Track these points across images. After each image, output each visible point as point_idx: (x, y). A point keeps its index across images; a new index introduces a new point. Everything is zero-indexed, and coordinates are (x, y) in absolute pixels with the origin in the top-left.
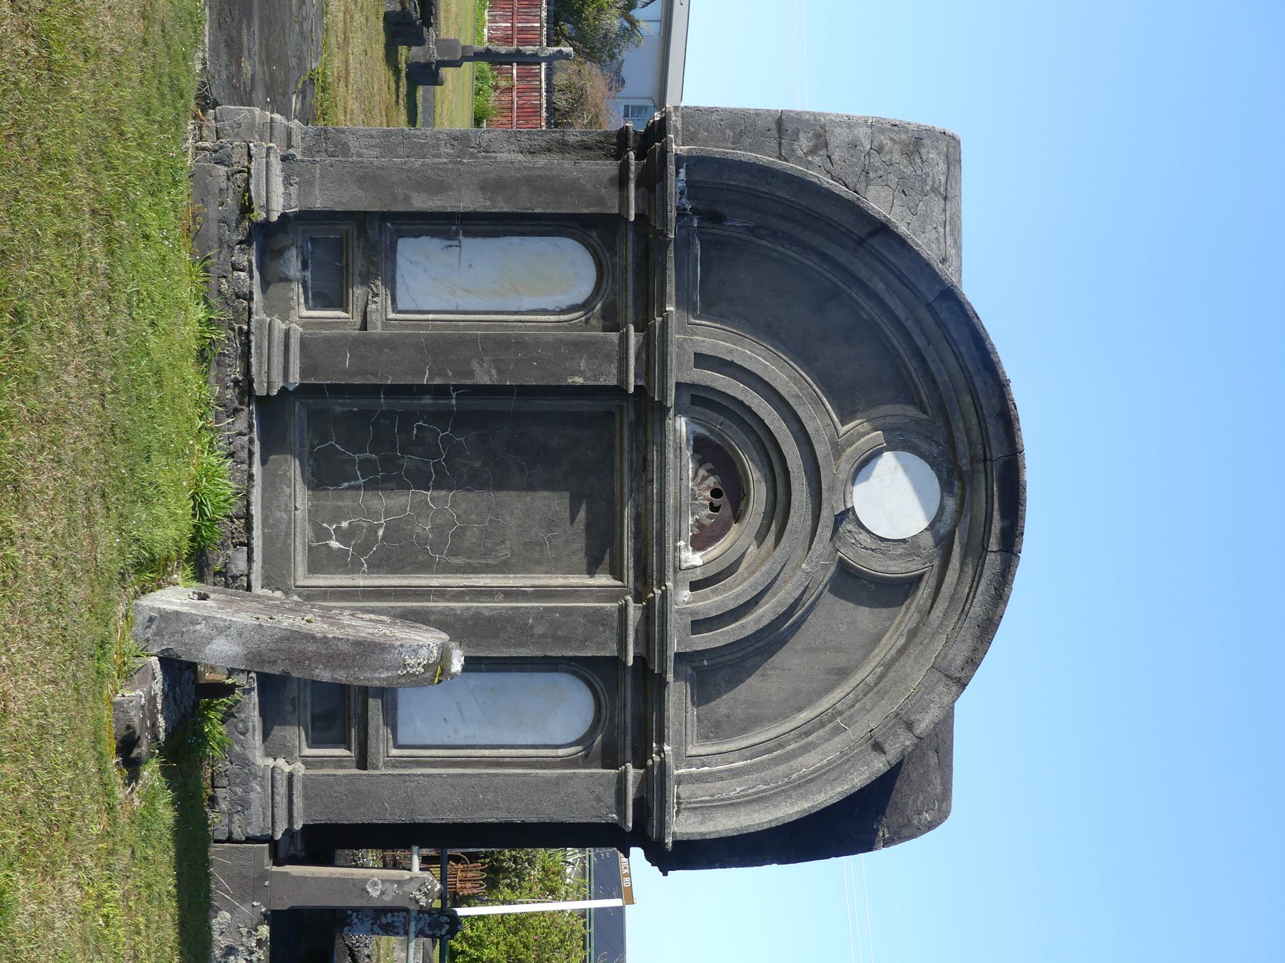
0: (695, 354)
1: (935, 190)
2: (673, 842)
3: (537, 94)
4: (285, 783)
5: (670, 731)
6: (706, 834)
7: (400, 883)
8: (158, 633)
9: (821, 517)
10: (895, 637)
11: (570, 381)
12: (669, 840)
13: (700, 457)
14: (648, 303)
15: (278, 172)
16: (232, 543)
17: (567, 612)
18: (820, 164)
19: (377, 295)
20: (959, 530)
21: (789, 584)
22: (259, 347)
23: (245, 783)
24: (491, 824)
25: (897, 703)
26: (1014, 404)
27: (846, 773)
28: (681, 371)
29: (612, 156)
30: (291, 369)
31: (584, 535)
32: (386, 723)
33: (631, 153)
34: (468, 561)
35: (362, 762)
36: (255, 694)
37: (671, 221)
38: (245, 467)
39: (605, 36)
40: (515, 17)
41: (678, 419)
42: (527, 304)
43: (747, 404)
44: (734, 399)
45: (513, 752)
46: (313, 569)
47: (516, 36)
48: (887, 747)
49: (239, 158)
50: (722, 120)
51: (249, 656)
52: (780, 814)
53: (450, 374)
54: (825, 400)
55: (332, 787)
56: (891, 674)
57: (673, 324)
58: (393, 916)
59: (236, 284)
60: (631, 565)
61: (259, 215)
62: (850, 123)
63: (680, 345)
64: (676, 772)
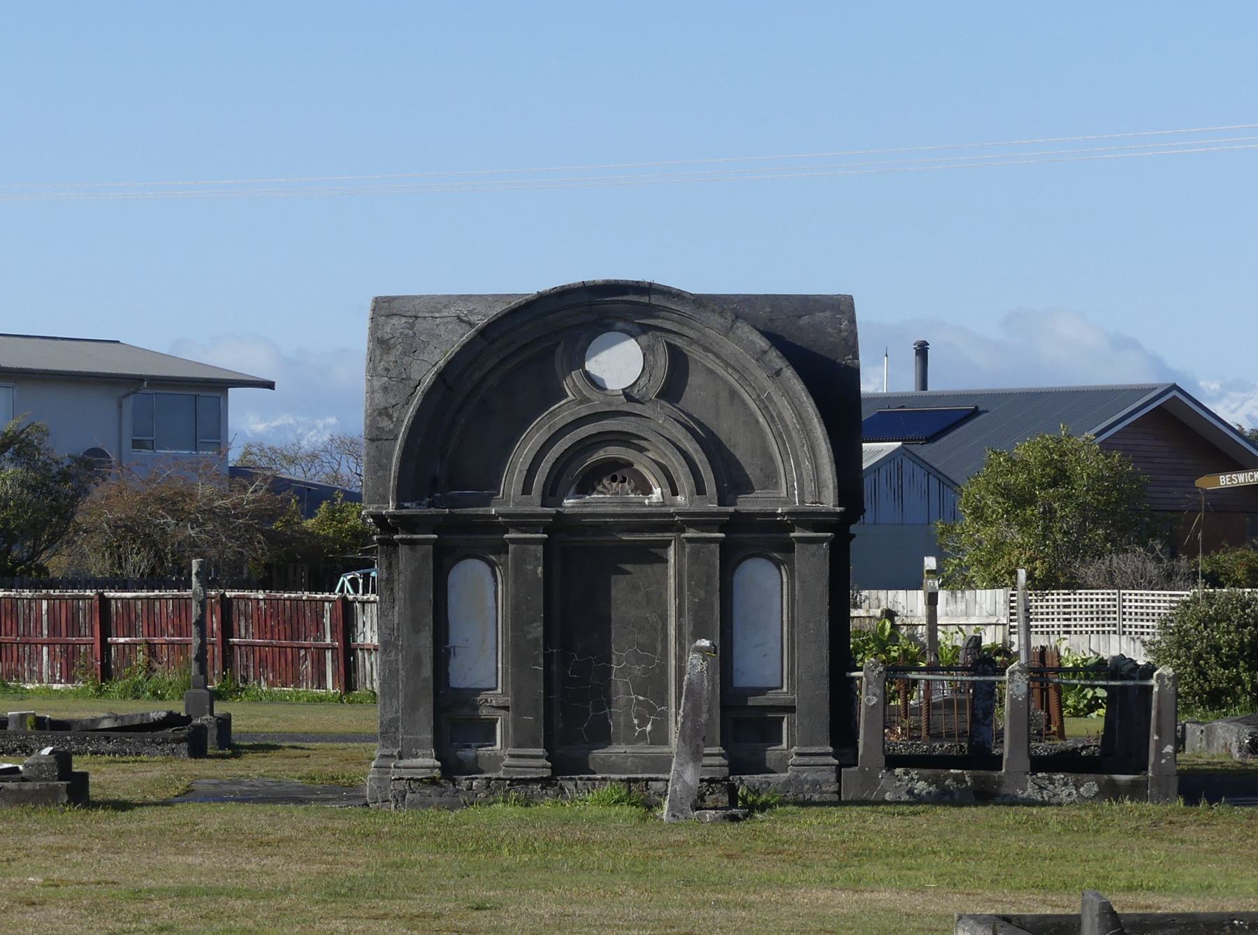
1: (412, 327)
3: (157, 604)
4: (803, 758)
7: (868, 683)
12: (838, 509)
14: (492, 526)
15: (410, 761)
17: (691, 577)
22: (520, 773)
23: (801, 783)
28: (533, 505)
30: (534, 753)
32: (764, 694)
33: (395, 537)
35: (790, 709)
36: (744, 777)
38: (597, 783)
39: (33, 489)
40: (33, 639)
42: (491, 603)
47: (63, 639)
48: (778, 367)
49: (401, 786)
52: (821, 437)
54: (552, 409)
57: (502, 509)
58: (977, 709)
60: (661, 534)
61: (437, 773)
62: (371, 391)
63: (517, 504)
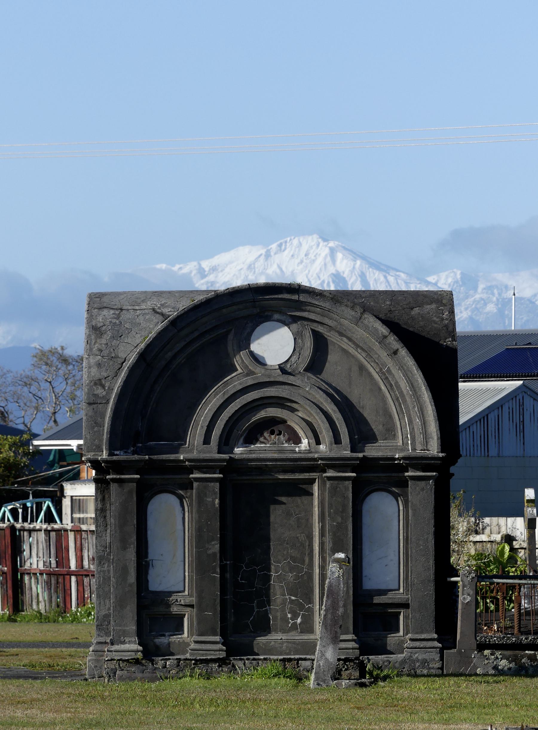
0: (204, 444)
2: (442, 453)
4: (414, 643)
5: (389, 454)
6: (438, 437)
7: (464, 586)
8: (324, 681)
9: (283, 381)
10: (343, 342)
11: (217, 506)
12: (441, 455)
13: (254, 441)
15: (119, 646)
16: (297, 668)
17: (331, 506)
18: (109, 383)
19: (177, 600)
20: (289, 312)
21: (317, 396)
22: (203, 655)
23: (414, 661)
24: (435, 542)
25: (375, 343)
26: (226, 290)
27: (408, 368)
29: (107, 486)
30: (213, 640)
31: (294, 498)
32: (386, 595)
33: (107, 477)
34: (307, 555)
35: (406, 606)
36: (370, 657)
37: (140, 458)
38: (260, 662)
41: (236, 452)
43: (228, 418)
44: (226, 425)
45: (401, 532)
46: (311, 631)
48: (395, 348)
49: (112, 665)
50: (89, 433)
51: (333, 643)
53: (215, 564)
54: (225, 380)
55: (417, 620)
56: (361, 345)
59: (172, 666)
60: (308, 474)
61: (140, 655)
63: (199, 452)
64: (410, 451)
